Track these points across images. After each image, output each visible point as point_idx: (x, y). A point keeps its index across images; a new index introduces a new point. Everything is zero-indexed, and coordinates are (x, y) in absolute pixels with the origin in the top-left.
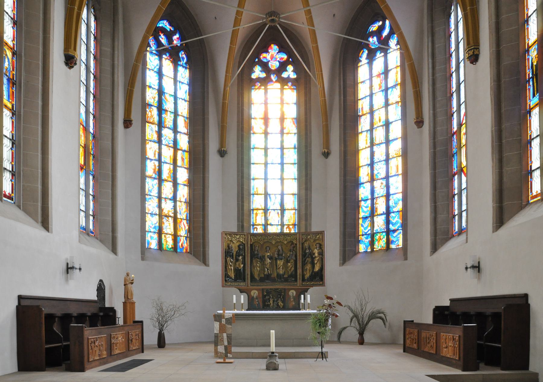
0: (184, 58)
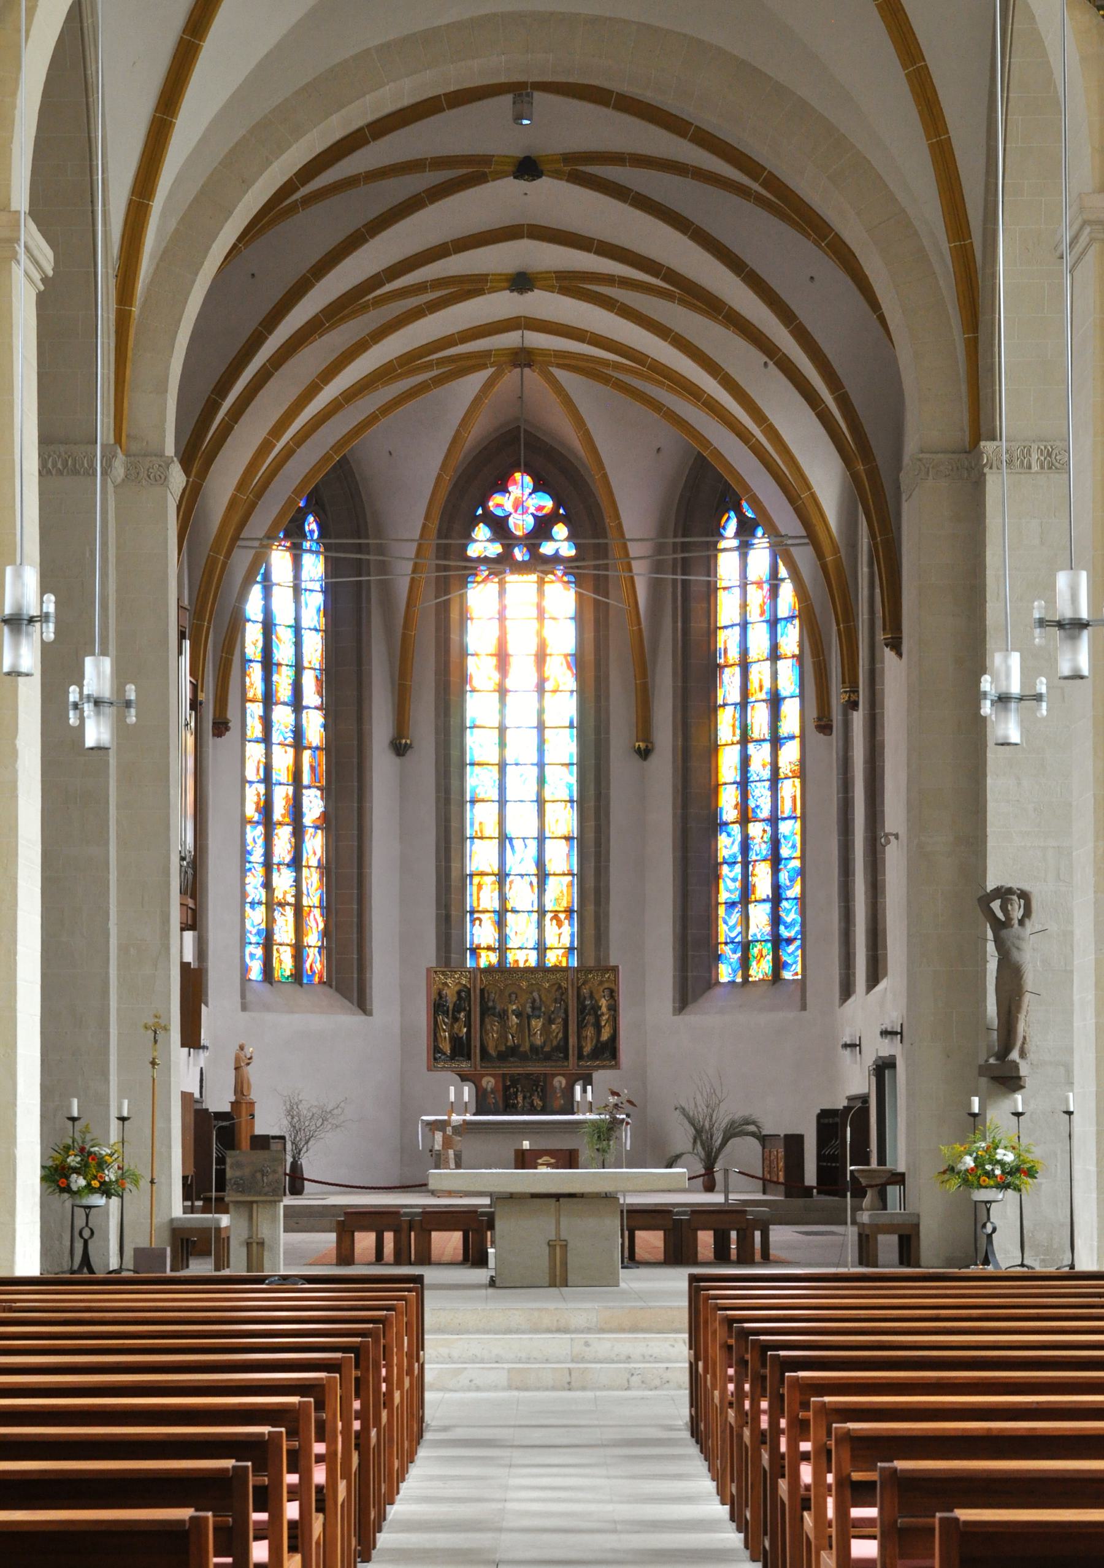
0: (314, 531)
